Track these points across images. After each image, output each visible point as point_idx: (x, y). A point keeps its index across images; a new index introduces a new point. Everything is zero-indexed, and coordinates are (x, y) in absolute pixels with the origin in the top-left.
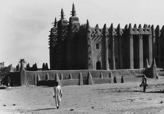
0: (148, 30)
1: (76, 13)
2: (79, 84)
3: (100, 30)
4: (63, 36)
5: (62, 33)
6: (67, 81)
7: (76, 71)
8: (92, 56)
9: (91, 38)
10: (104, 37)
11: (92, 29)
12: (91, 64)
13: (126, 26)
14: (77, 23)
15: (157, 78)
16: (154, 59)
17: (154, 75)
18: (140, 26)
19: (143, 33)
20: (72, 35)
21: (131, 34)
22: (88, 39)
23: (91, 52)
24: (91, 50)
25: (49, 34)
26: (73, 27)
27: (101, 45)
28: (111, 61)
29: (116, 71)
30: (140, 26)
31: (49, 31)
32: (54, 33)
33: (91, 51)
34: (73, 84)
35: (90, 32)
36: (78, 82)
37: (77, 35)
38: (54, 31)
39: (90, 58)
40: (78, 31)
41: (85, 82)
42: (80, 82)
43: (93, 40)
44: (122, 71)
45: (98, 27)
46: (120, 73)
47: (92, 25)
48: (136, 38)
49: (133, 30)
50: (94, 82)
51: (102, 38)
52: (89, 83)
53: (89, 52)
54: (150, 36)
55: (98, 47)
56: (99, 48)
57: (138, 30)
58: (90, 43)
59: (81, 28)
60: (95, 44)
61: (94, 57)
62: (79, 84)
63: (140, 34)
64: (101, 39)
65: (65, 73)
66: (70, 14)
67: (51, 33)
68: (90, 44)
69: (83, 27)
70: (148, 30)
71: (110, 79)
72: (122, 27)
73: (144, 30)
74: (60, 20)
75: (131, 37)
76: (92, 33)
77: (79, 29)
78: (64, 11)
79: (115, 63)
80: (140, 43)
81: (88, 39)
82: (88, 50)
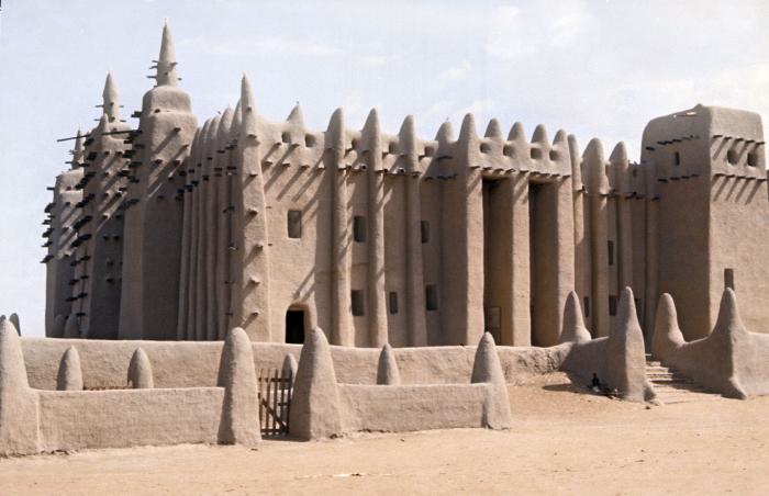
0: (554, 155)
1: (176, 73)
2: (226, 437)
3: (310, 140)
4: (106, 217)
5: (104, 183)
6: (121, 394)
7: (176, 346)
8: (262, 272)
9: (262, 179)
10: (330, 172)
11: (270, 129)
12: (258, 318)
13: (443, 133)
14: (181, 118)
15: (649, 396)
16: (629, 289)
17: (632, 380)
18: (515, 132)
19: (533, 166)
20: (153, 178)
21: (474, 165)
22: (244, 179)
23: (258, 249)
24: (263, 238)
25: (50, 198)
26: (159, 137)
27: (315, 219)
28: (363, 304)
29: (414, 357)
30: (515, 132)
31: (49, 189)
32: (71, 196)
33: (261, 243)
34: (162, 434)
35: (257, 144)
36: (215, 415)
37: (182, 179)
38: (69, 189)
39: (253, 284)
40: (186, 159)
41: (277, 419)
42: (235, 415)
43: (274, 191)
44: (445, 354)
45: (300, 122)
46: (435, 368)
47: (268, 118)
48: (494, 186)
49: (484, 148)
50: (353, 416)
51: (323, 181)
52: (314, 425)
53: (248, 248)
54: (563, 186)
55: (295, 230)
56: (304, 231)
57: (507, 151)
58: (256, 200)
59: (205, 137)
60: (280, 212)
61: (280, 271)
62: (220, 435)
63: (517, 173)
64: (316, 184)
65: (107, 355)
66: (149, 77)
67: (57, 196)
68: (255, 209)
69: (217, 127)
70: (554, 155)
71: (486, 392)
72: (425, 136)
73: (535, 153)
74: (96, 124)
75: (476, 183)
76: (267, 151)
77: (189, 148)
78: (117, 88)
79: (385, 316)
80: (515, 217)
81: (244, 179)
82: (242, 238)
